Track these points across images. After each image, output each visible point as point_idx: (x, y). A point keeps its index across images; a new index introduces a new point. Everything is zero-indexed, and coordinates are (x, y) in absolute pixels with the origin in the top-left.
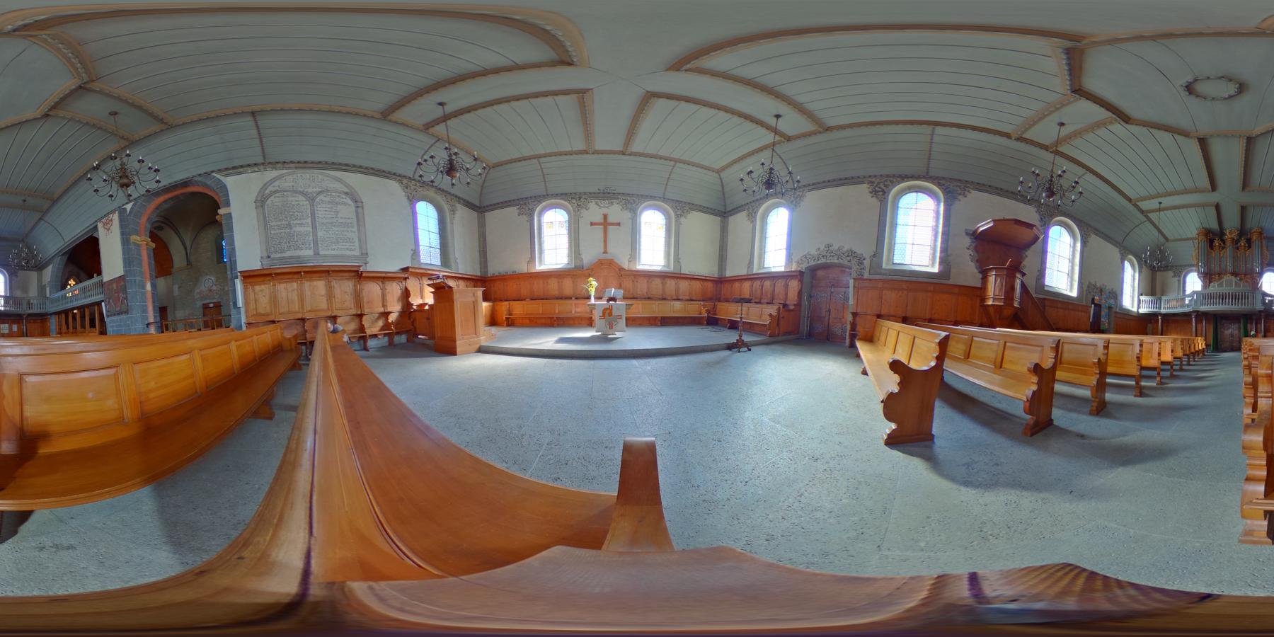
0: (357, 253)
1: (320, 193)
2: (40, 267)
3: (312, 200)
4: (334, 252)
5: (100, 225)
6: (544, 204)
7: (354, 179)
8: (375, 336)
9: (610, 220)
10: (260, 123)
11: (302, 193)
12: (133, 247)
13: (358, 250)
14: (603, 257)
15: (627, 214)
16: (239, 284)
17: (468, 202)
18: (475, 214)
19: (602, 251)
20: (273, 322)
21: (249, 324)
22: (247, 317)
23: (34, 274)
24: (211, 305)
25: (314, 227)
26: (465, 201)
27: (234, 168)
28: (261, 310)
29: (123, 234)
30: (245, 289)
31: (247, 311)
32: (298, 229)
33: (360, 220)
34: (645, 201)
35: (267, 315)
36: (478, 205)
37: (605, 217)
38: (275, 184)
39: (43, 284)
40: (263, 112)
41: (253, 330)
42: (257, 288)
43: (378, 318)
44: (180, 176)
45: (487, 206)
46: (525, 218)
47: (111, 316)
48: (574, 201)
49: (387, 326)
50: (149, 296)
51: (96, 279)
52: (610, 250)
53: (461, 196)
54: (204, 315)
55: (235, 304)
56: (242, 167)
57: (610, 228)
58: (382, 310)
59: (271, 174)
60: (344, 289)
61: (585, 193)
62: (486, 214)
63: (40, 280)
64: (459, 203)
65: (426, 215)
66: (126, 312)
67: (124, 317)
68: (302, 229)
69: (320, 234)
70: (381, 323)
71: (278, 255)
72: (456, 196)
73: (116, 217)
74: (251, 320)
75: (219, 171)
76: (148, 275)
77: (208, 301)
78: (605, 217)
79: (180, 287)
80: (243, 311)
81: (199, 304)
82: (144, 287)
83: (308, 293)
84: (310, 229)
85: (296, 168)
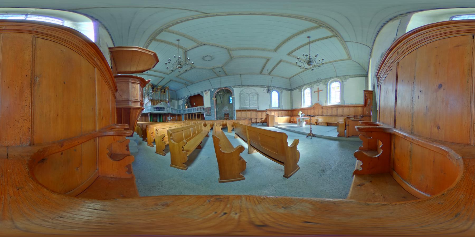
0: (257, 106)
1: (251, 93)
2: (178, 100)
3: (249, 95)
4: (253, 107)
5: (204, 93)
6: (304, 87)
7: (257, 89)
8: (259, 123)
9: (320, 89)
10: (241, 76)
11: (247, 93)
12: (213, 100)
13: (257, 105)
14: (317, 102)
15: (325, 86)
16: (235, 112)
17: (287, 89)
18: (289, 92)
19: (317, 100)
20: (246, 119)
21: (237, 119)
22: (236, 118)
23: (176, 101)
24: (227, 114)
25: (249, 101)
26: (285, 89)
27: (236, 86)
28: (239, 117)
29: (211, 97)
30: (236, 113)
31: (236, 117)
32: (246, 102)
33: (258, 99)
34: (330, 80)
35: (240, 118)
36: (291, 89)
37: (318, 89)
38: (243, 91)
39: (179, 105)
40: (242, 74)
41: (237, 120)
42: (238, 113)
43: (260, 119)
44: (225, 86)
45: (293, 89)
46: (300, 92)
47: (206, 116)
48: (311, 85)
49: (262, 121)
50: (215, 112)
51: (202, 107)
52: (320, 100)
53: (284, 88)
54: (225, 117)
55: (234, 115)
56: (237, 86)
57: (320, 92)
58: (261, 118)
59: (242, 88)
60: (254, 113)
61: (313, 82)
62: (293, 91)
63: (178, 103)
64: (284, 90)
65: (275, 95)
66: (211, 115)
67: (210, 116)
68: (247, 102)
69: (250, 103)
70: (261, 120)
71: (243, 107)
72: (283, 88)
73: (209, 92)
74: (237, 118)
75: (233, 86)
76: (215, 107)
77: (226, 113)
78: (318, 89)
79: (219, 109)
80: (236, 117)
81: (224, 113)
82: (214, 110)
83: (247, 114)
84: (248, 102)
85: (247, 87)
